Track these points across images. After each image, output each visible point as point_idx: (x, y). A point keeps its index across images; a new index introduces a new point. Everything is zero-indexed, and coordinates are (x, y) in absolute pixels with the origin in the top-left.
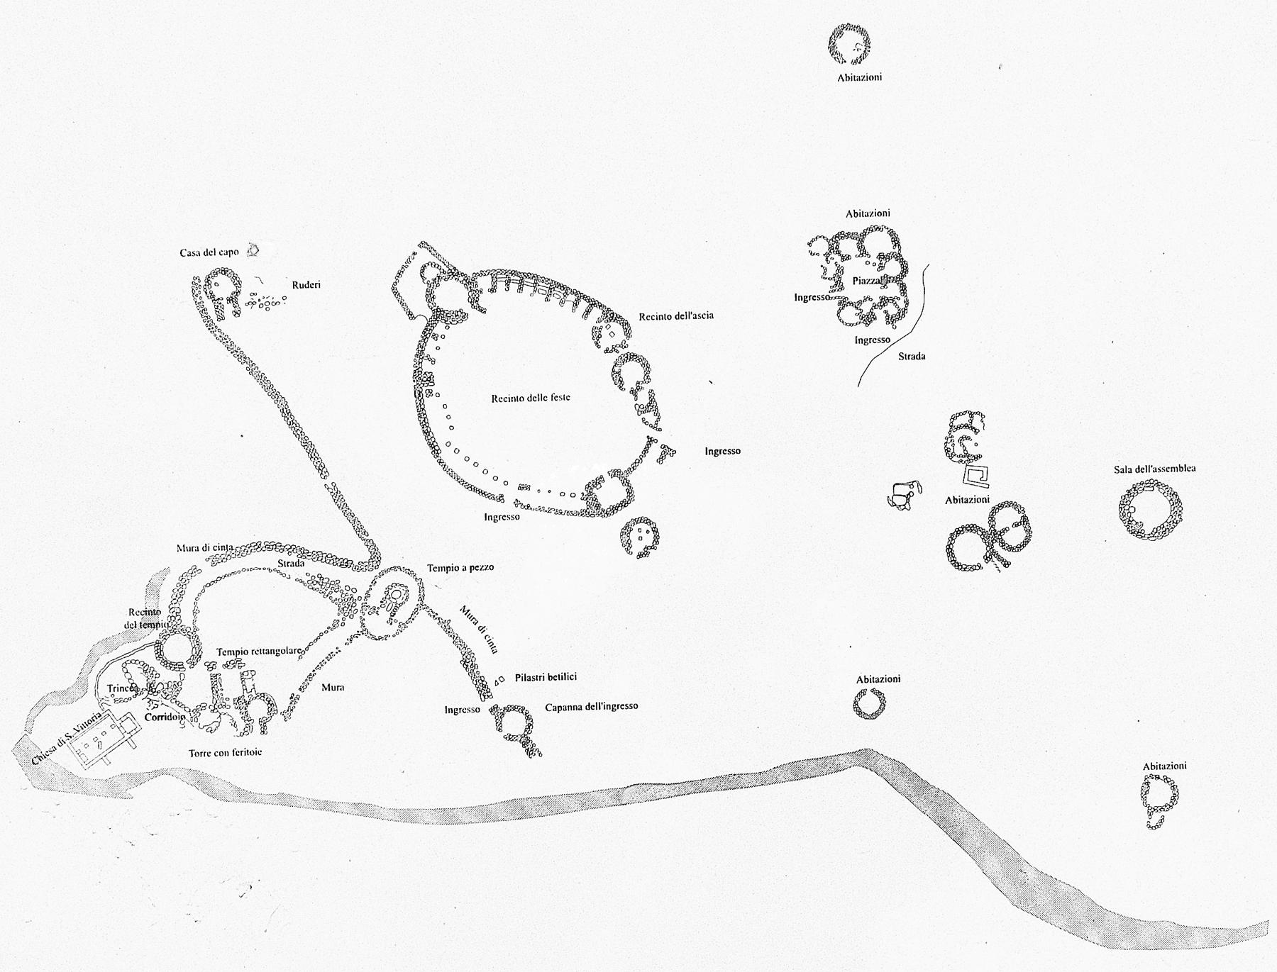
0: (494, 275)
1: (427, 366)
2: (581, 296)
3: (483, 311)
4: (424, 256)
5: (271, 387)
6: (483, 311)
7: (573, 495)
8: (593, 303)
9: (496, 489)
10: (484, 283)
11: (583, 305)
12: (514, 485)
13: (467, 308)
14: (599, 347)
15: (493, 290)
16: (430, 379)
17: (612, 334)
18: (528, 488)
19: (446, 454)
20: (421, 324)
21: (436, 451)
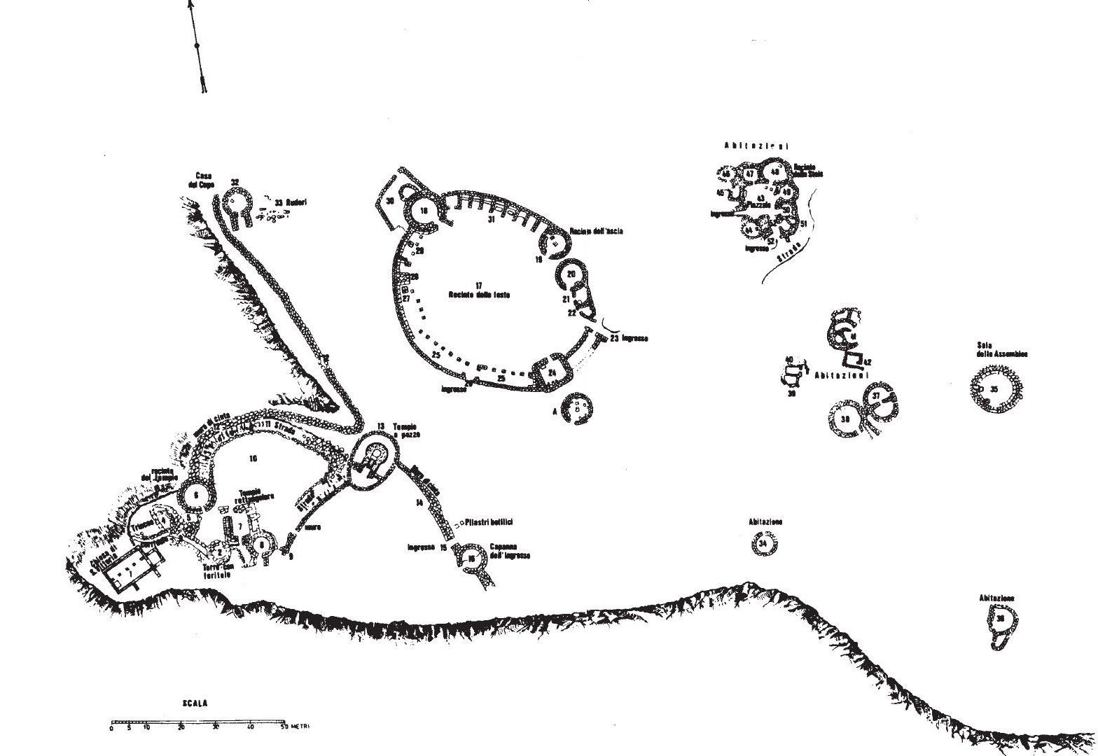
4: (403, 179)
6: (450, 224)
12: (473, 366)
13: (437, 222)
15: (459, 207)
18: (485, 367)
20: (400, 233)
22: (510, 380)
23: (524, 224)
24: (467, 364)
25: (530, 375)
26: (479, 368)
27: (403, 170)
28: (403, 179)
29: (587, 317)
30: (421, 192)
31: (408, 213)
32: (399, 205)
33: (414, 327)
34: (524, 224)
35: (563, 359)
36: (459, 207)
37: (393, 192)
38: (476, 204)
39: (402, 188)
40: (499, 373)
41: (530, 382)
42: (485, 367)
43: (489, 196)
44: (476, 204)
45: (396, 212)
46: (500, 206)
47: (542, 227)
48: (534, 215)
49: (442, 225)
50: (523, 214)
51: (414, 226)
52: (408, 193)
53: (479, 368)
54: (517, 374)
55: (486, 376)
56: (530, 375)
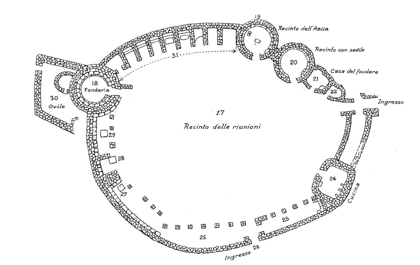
0: (119, 52)
1: (107, 167)
2: (205, 27)
3: (130, 87)
4: (50, 72)
5: (171, 243)
6: (130, 87)
7: (306, 202)
8: (220, 27)
9: (236, 235)
10: (116, 63)
11: (213, 33)
12: (251, 223)
13: (113, 92)
14: (250, 56)
15: (126, 66)
16: (115, 177)
17: (257, 41)
18: (265, 218)
19: (165, 234)
20: (81, 127)
21: (152, 234)
22: (295, 216)
23: (206, 42)
24: (243, 224)
25: (314, 199)
26: (259, 221)
27: (41, 60)
28: (50, 72)
29: (337, 100)
30: (82, 71)
31: (79, 102)
32: (65, 99)
33: (155, 223)
34: (206, 42)
35: (335, 161)
36: (126, 66)
37: (48, 89)
38: (185, 44)
39: (56, 82)
40: (280, 216)
41: (314, 208)
42: (265, 218)
43: (139, 39)
44: (185, 44)
45: (69, 111)
46: (184, 36)
47: (229, 36)
48: (212, 26)
49: (122, 92)
50: (198, 33)
51: (93, 111)
52: (65, 82)
53: (259, 221)
54: (300, 204)
55: (269, 226)
56: (314, 199)
